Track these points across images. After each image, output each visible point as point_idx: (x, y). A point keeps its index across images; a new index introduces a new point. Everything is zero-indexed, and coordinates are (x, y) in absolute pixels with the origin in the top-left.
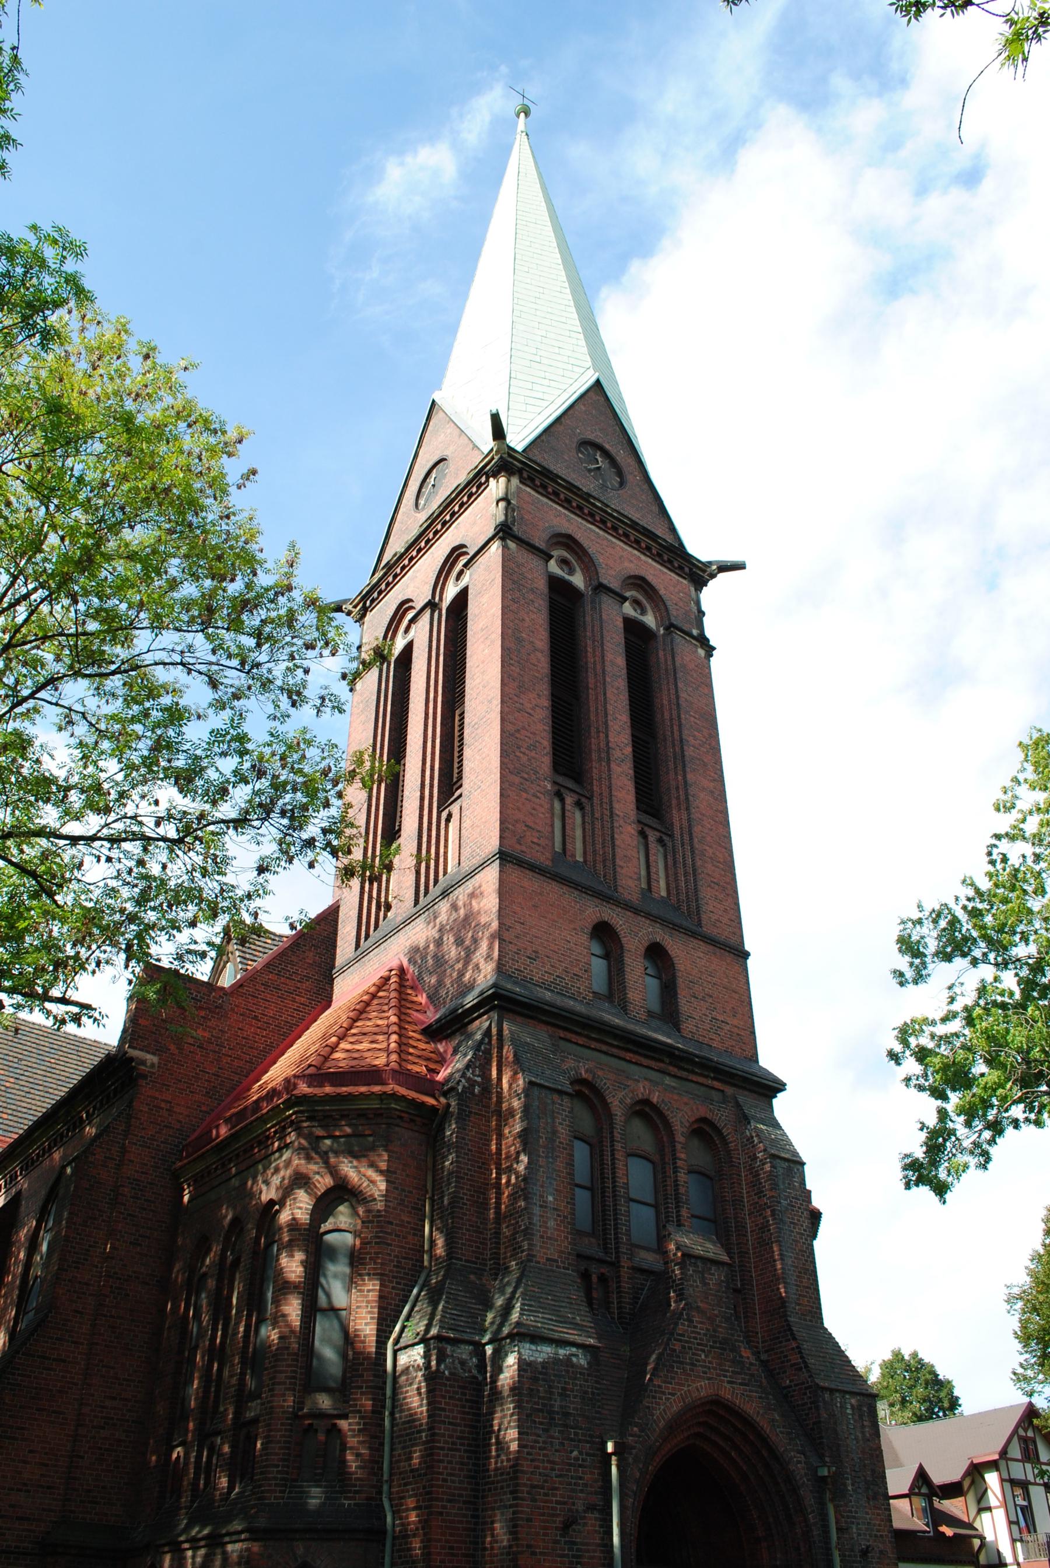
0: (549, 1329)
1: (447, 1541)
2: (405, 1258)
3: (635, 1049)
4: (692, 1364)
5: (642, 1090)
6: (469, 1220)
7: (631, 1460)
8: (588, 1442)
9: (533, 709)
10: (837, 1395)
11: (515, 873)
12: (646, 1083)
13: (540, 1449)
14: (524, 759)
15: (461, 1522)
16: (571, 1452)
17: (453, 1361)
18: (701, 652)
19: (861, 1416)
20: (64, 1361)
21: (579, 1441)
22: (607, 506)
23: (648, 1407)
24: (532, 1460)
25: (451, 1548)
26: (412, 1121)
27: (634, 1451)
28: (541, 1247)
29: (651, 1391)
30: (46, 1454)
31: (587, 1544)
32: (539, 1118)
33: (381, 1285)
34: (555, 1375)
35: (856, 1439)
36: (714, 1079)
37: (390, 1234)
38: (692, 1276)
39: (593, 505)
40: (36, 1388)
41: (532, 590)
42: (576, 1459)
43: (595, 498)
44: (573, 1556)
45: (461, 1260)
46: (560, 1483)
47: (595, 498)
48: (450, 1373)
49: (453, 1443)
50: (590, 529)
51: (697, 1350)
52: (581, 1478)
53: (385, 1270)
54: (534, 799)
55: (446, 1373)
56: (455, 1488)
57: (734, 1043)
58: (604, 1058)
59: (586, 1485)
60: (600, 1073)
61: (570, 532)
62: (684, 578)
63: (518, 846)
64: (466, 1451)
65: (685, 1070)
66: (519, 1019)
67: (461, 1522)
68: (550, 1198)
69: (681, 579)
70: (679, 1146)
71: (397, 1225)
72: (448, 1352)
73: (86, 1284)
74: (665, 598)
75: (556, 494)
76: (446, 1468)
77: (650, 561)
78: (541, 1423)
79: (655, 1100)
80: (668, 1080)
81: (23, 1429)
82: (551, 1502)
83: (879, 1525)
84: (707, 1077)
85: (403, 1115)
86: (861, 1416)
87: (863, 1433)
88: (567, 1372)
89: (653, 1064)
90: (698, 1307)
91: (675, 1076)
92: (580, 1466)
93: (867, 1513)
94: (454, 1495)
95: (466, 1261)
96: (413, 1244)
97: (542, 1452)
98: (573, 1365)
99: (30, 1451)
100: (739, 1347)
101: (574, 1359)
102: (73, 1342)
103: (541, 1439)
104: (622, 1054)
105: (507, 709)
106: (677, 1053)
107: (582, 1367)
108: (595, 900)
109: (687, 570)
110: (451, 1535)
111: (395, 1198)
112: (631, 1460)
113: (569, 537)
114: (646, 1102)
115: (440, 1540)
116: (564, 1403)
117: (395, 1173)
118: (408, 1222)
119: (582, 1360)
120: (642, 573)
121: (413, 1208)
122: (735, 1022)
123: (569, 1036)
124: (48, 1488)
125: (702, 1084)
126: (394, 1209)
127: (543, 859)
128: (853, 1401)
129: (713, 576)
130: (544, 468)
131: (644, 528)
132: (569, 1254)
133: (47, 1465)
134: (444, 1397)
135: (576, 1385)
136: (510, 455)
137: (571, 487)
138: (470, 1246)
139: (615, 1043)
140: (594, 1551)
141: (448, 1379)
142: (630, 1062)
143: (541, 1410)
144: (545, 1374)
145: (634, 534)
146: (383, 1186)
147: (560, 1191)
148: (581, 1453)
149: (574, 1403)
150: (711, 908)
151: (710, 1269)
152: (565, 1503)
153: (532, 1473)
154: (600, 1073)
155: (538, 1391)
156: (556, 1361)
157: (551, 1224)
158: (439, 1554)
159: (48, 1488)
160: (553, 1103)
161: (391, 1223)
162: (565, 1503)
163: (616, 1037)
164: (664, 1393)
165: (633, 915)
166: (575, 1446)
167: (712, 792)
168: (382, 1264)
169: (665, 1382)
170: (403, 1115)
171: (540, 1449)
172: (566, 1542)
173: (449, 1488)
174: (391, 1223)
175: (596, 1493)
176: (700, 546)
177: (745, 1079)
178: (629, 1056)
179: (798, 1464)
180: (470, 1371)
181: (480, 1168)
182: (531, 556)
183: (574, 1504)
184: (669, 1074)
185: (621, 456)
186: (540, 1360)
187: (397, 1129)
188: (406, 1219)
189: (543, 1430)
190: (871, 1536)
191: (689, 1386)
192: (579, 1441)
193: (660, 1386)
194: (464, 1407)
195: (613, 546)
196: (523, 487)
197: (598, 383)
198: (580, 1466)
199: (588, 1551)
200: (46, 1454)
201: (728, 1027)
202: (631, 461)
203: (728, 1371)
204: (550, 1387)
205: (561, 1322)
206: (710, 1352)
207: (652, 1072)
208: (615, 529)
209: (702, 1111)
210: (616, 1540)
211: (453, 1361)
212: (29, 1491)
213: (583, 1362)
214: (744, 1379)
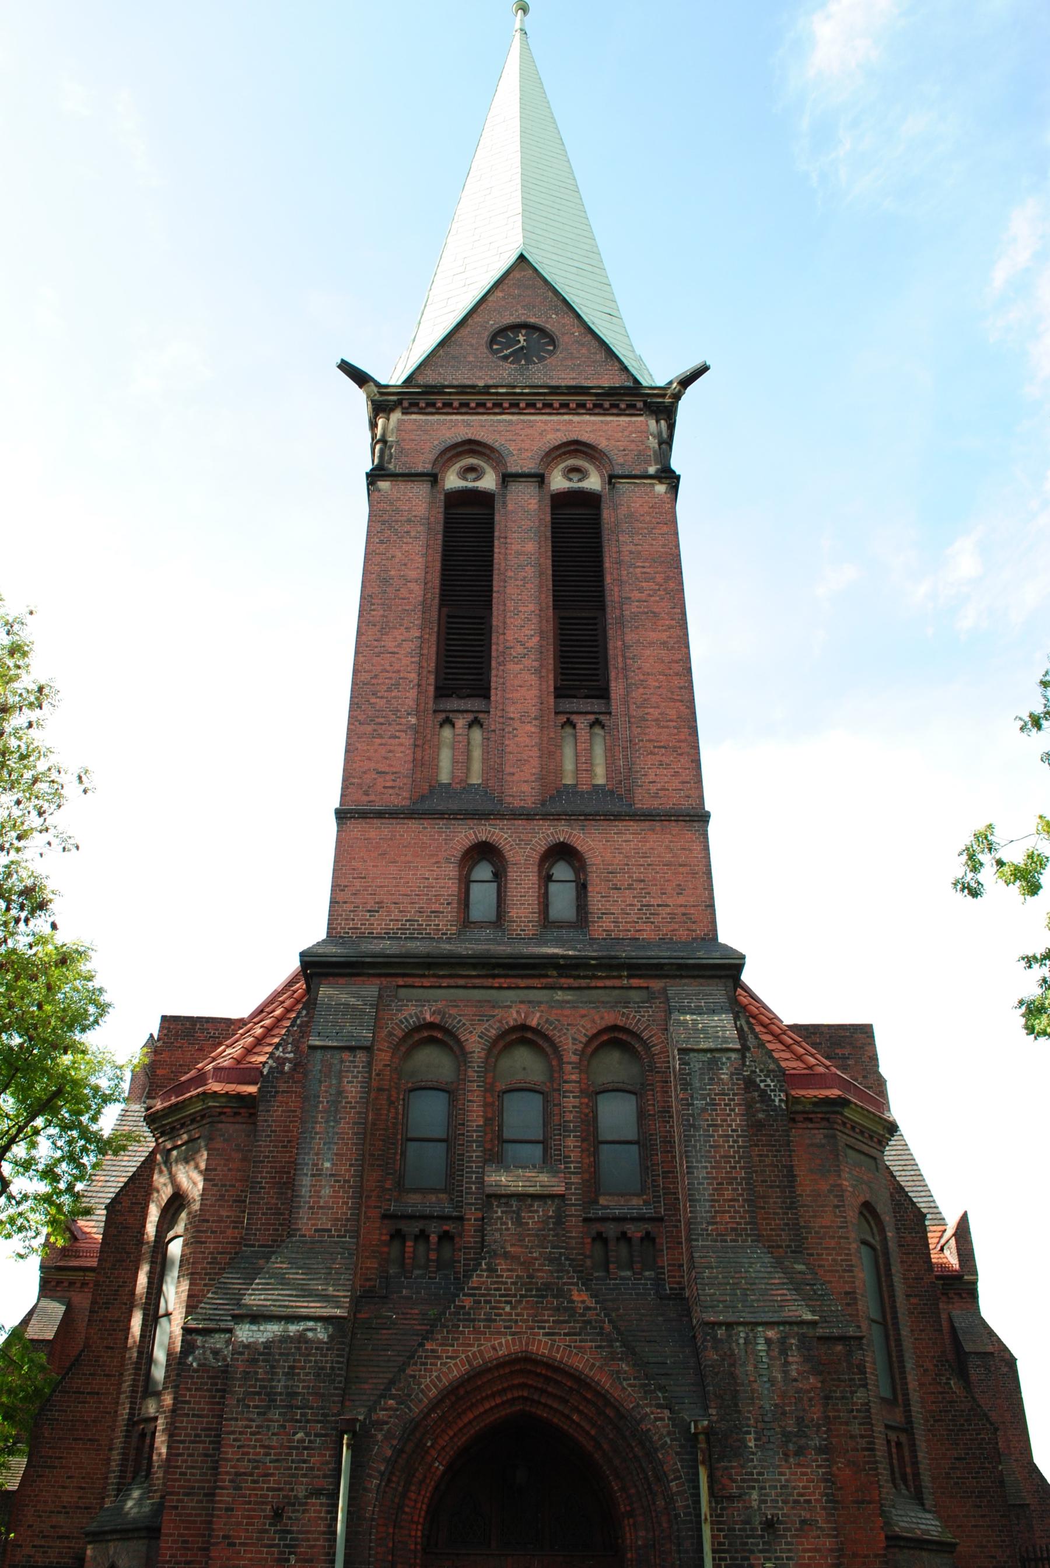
0: (280, 1306)
1: (180, 1535)
2: (221, 1253)
3: (503, 972)
4: (490, 1320)
5: (513, 1016)
6: (266, 1204)
7: (380, 1437)
8: (318, 1422)
9: (399, 646)
10: (741, 1328)
11: (356, 828)
12: (519, 1005)
13: (252, 1434)
14: (381, 703)
15: (200, 1515)
16: (295, 1434)
17: (204, 1353)
18: (661, 488)
19: (784, 1352)
20: (98, 1394)
21: (308, 1421)
22: (514, 387)
23: (414, 1376)
24: (239, 1447)
25: (186, 1542)
26: (236, 1114)
27: (386, 1427)
28: (309, 1219)
29: (420, 1357)
30: (83, 1478)
31: (308, 1532)
32: (320, 1082)
33: (191, 1284)
34: (280, 1354)
35: (772, 1381)
36: (629, 977)
37: (205, 1232)
38: (501, 1218)
39: (497, 394)
40: (72, 1421)
41: (409, 521)
42: (302, 1441)
43: (496, 387)
44: (286, 1546)
45: (253, 1246)
46: (276, 1468)
47: (496, 387)
48: (199, 1365)
49: (196, 1435)
50: (499, 421)
51: (500, 1302)
52: (305, 1462)
53: (196, 1268)
54: (392, 741)
55: (195, 1364)
56: (196, 1481)
57: (676, 926)
58: (461, 993)
59: (312, 1469)
60: (453, 1011)
61: (469, 436)
62: (641, 415)
63: (365, 798)
64: (211, 1442)
65: (585, 977)
66: (341, 980)
67: (200, 1515)
68: (327, 1165)
69: (634, 419)
70: (568, 1068)
71: (213, 1222)
72: (199, 1343)
73: (117, 1321)
74: (606, 450)
75: (448, 405)
76: (186, 1461)
77: (587, 417)
78: (256, 1407)
79: (534, 1023)
80: (559, 995)
81: (61, 1458)
82: (262, 1489)
83: (804, 1488)
84: (620, 977)
85: (225, 1110)
86: (784, 1352)
87: (786, 1373)
88: (299, 1349)
89: (535, 982)
90: (506, 1253)
91: (570, 988)
92: (305, 1448)
93: (782, 1474)
94: (193, 1488)
95: (260, 1246)
96: (233, 1238)
97: (254, 1437)
98: (307, 1341)
99: (68, 1477)
100: (570, 1290)
101: (310, 1334)
102: (105, 1375)
103: (254, 1424)
104: (489, 982)
105: (361, 659)
106: (562, 962)
107: (321, 1342)
108: (469, 822)
109: (640, 405)
110: (186, 1528)
111: (213, 1195)
112: (380, 1437)
113: (470, 441)
114: (524, 1027)
115: (171, 1535)
116: (290, 1383)
117: (215, 1170)
118: (228, 1217)
119: (321, 1334)
120: (573, 436)
121: (235, 1201)
122: (681, 900)
123: (410, 981)
124: (86, 1508)
125: (614, 988)
126: (211, 1206)
127: (399, 800)
128: (770, 1334)
129: (677, 397)
130: (426, 386)
131: (568, 387)
132: (348, 1220)
133: (84, 1488)
134: (190, 1390)
135: (310, 1361)
136: (382, 394)
137: (463, 389)
138: (265, 1230)
139: (474, 973)
140: (318, 1540)
141: (196, 1371)
142: (500, 988)
143: (259, 1393)
144: (269, 1354)
145: (556, 400)
146: (201, 1185)
147: (342, 1155)
148: (307, 1434)
149: (304, 1381)
150: (652, 778)
151: (532, 1206)
152: (280, 1489)
153: (238, 1460)
154: (453, 1011)
155: (256, 1373)
156: (285, 1339)
157: (326, 1191)
158: (170, 1548)
159: (86, 1508)
160: (342, 1061)
161: (208, 1221)
162: (280, 1489)
163: (474, 966)
164: (439, 1358)
165: (524, 822)
166: (300, 1428)
167: (664, 643)
168: (193, 1263)
169: (441, 1345)
170: (225, 1110)
171: (252, 1434)
172: (275, 1532)
173: (189, 1480)
174: (208, 1221)
175: (325, 1476)
176: (657, 371)
177: (680, 966)
178: (496, 982)
179: (658, 1422)
180: (225, 1360)
181: (286, 1147)
182: (410, 485)
183: (292, 1490)
184: (561, 988)
185: (552, 322)
186: (261, 1340)
187: (220, 1125)
188: (225, 1214)
189: (258, 1414)
190: (785, 1502)
191: (480, 1345)
192: (308, 1421)
193: (433, 1351)
194: (214, 1397)
195: (531, 425)
196: (406, 417)
197: (522, 258)
198: (305, 1448)
199: (308, 1540)
200: (83, 1478)
201: (664, 912)
202: (569, 320)
203: (548, 1321)
204: (273, 1367)
205: (304, 1296)
206: (520, 1302)
207: (536, 991)
208: (531, 405)
209: (610, 1018)
210: (340, 1526)
211: (204, 1353)
212: (68, 1513)
213: (322, 1336)
214: (574, 1328)
